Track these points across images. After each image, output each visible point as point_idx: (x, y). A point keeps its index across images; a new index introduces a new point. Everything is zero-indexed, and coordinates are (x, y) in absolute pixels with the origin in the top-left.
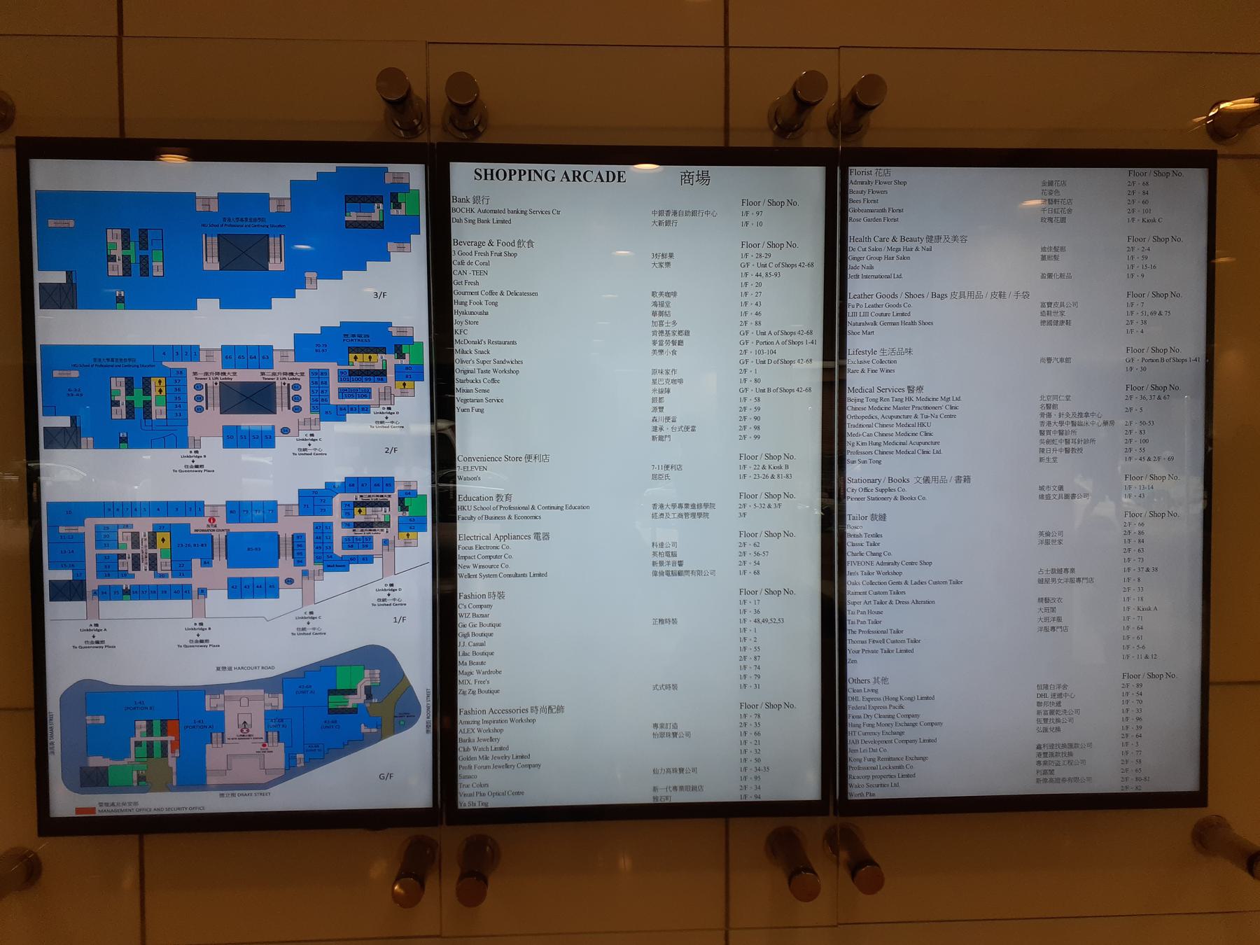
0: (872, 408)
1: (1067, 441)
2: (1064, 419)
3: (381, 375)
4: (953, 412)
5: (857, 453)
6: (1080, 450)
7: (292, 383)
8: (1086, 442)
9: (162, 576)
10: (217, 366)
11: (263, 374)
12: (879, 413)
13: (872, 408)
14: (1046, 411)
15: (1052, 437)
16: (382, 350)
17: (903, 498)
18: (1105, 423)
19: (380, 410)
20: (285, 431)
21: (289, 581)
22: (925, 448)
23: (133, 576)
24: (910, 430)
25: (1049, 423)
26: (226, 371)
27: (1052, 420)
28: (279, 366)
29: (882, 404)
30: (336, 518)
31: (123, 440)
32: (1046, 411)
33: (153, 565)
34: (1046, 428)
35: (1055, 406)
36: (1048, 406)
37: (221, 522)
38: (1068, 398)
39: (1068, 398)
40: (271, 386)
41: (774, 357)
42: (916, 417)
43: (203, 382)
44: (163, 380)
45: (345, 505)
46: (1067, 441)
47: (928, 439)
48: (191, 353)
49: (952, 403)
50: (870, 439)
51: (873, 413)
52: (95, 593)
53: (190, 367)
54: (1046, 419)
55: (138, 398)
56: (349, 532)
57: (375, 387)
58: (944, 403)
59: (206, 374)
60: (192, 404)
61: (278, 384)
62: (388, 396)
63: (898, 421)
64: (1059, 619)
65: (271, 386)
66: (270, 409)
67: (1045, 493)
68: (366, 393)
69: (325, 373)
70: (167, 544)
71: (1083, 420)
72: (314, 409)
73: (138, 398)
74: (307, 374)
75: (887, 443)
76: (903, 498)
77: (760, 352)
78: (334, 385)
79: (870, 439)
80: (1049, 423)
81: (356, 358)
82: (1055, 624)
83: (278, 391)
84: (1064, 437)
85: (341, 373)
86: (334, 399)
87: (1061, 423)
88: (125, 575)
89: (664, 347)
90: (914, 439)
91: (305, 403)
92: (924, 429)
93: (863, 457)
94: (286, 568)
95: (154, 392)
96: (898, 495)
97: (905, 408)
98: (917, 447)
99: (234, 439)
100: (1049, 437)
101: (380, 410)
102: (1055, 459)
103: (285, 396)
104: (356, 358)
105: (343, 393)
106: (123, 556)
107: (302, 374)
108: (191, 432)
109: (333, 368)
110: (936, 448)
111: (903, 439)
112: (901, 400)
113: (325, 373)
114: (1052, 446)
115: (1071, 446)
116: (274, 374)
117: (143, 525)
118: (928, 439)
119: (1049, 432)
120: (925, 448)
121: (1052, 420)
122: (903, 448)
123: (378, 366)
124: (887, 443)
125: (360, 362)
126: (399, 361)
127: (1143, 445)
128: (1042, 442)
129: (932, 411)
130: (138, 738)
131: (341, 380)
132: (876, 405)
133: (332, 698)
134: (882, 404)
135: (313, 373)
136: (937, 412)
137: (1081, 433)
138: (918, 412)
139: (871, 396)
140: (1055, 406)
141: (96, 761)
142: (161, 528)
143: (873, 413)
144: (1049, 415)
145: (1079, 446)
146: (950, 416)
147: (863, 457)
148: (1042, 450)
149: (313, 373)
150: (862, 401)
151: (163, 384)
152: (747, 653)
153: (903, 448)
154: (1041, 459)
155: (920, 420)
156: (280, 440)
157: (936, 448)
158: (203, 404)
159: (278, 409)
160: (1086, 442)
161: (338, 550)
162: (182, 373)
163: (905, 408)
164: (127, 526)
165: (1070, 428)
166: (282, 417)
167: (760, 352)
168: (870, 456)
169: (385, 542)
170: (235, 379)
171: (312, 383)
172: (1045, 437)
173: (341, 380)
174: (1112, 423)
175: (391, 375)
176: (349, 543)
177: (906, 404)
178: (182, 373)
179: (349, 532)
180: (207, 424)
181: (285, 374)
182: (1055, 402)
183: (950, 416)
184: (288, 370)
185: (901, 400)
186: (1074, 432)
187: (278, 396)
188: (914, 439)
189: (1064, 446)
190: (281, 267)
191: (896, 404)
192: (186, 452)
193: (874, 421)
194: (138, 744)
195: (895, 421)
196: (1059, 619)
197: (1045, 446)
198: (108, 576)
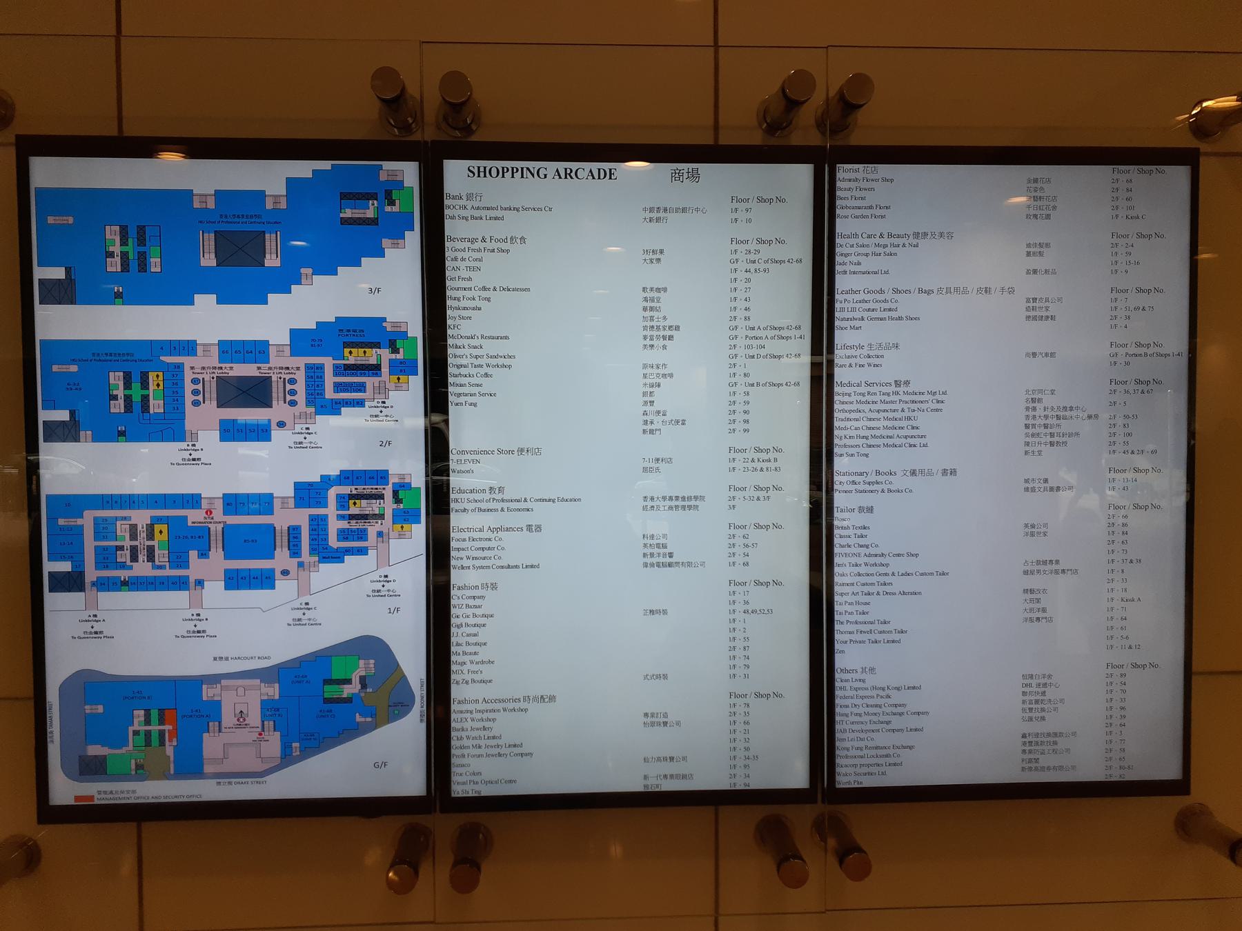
1: (1052, 435)
2: (1049, 413)
3: (375, 369)
4: (939, 406)
5: (845, 446)
6: (1065, 443)
7: (288, 377)
8: (1070, 435)
9: (160, 567)
10: (214, 360)
11: (259, 368)
12: (866, 407)
14: (1031, 405)
15: (1037, 430)
16: (377, 345)
17: (890, 491)
18: (1090, 417)
19: (375, 403)
20: (281, 425)
21: (285, 573)
22: (912, 441)
23: (131, 568)
24: (897, 424)
25: (1034, 417)
26: (223, 365)
27: (1037, 414)
28: (275, 361)
29: (869, 398)
30: (331, 510)
32: (1031, 405)
33: (151, 557)
34: (1031, 422)
35: (1040, 400)
36: (1033, 400)
37: (218, 514)
38: (1053, 392)
39: (1053, 392)
40: (267, 380)
41: (763, 352)
42: (903, 410)
43: (200, 377)
44: (161, 374)
45: (340, 497)
46: (1052, 435)
47: (915, 432)
48: (188, 347)
49: (938, 397)
50: (858, 432)
51: (861, 407)
52: (93, 584)
53: (187, 361)
54: (1031, 413)
55: (136, 392)
56: (344, 524)
57: (370, 381)
58: (931, 397)
59: (203, 368)
60: (189, 398)
61: (274, 378)
62: (382, 390)
63: (885, 414)
64: (1044, 610)
65: (267, 380)
66: (266, 403)
67: (1030, 486)
68: (361, 388)
69: (321, 367)
70: (165, 536)
71: (1068, 413)
72: (309, 403)
73: (136, 392)
74: (303, 369)
75: (875, 437)
76: (890, 491)
77: (749, 347)
78: (330, 379)
79: (858, 432)
80: (1034, 417)
81: (351, 353)
82: (1040, 615)
83: (274, 385)
84: (1049, 431)
85: (336, 367)
86: (329, 393)
87: (1046, 417)
88: (123, 566)
89: (655, 342)
90: (901, 433)
91: (301, 397)
92: (910, 423)
93: (851, 451)
94: (282, 559)
95: (152, 386)
96: (886, 487)
97: (892, 402)
98: (904, 441)
100: (1034, 431)
101: (375, 403)
102: (1040, 453)
103: (281, 390)
104: (351, 353)
105: (339, 387)
106: (121, 548)
107: (298, 368)
109: (328, 363)
110: (923, 441)
111: (890, 433)
112: (888, 394)
113: (321, 367)
114: (1037, 440)
115: (1056, 439)
116: (270, 368)
117: (141, 518)
118: (915, 432)
119: (1034, 426)
120: (912, 441)
121: (1037, 414)
122: (890, 441)
123: (373, 361)
124: (875, 437)
125: (354, 356)
126: (393, 356)
127: (1127, 439)
128: (1027, 435)
129: (919, 405)
130: (136, 727)
131: (336, 375)
132: (864, 399)
134: (869, 398)
135: (309, 367)
136: (924, 406)
137: (1066, 426)
138: (905, 406)
139: (859, 390)
140: (1040, 400)
141: (94, 750)
142: (159, 520)
143: (861, 407)
144: (1034, 409)
145: (1064, 439)
146: (937, 410)
147: (851, 451)
148: (1027, 444)
149: (309, 367)
150: (849, 395)
151: (161, 378)
153: (890, 441)
154: (1026, 453)
155: (907, 414)
157: (923, 441)
158: (200, 398)
159: (274, 403)
160: (1070, 435)
161: (333, 542)
162: (179, 367)
163: (892, 402)
164: (125, 518)
165: (1055, 421)
166: (278, 411)
167: (749, 347)
168: (857, 450)
169: (380, 534)
170: (231, 374)
171: (307, 377)
172: (1031, 431)
173: (336, 375)
174: (1096, 416)
175: (385, 369)
176: (344, 535)
177: (893, 398)
178: (179, 367)
179: (344, 524)
180: (204, 418)
181: (281, 368)
182: (1040, 396)
183: (937, 410)
184: (284, 364)
185: (888, 394)
186: (1058, 425)
187: (274, 390)
188: (901, 433)
189: (1049, 439)
190: (277, 263)
191: (883, 398)
193: (861, 415)
194: (136, 733)
195: (882, 415)
196: (1044, 610)
197: (1030, 440)
198: (106, 567)
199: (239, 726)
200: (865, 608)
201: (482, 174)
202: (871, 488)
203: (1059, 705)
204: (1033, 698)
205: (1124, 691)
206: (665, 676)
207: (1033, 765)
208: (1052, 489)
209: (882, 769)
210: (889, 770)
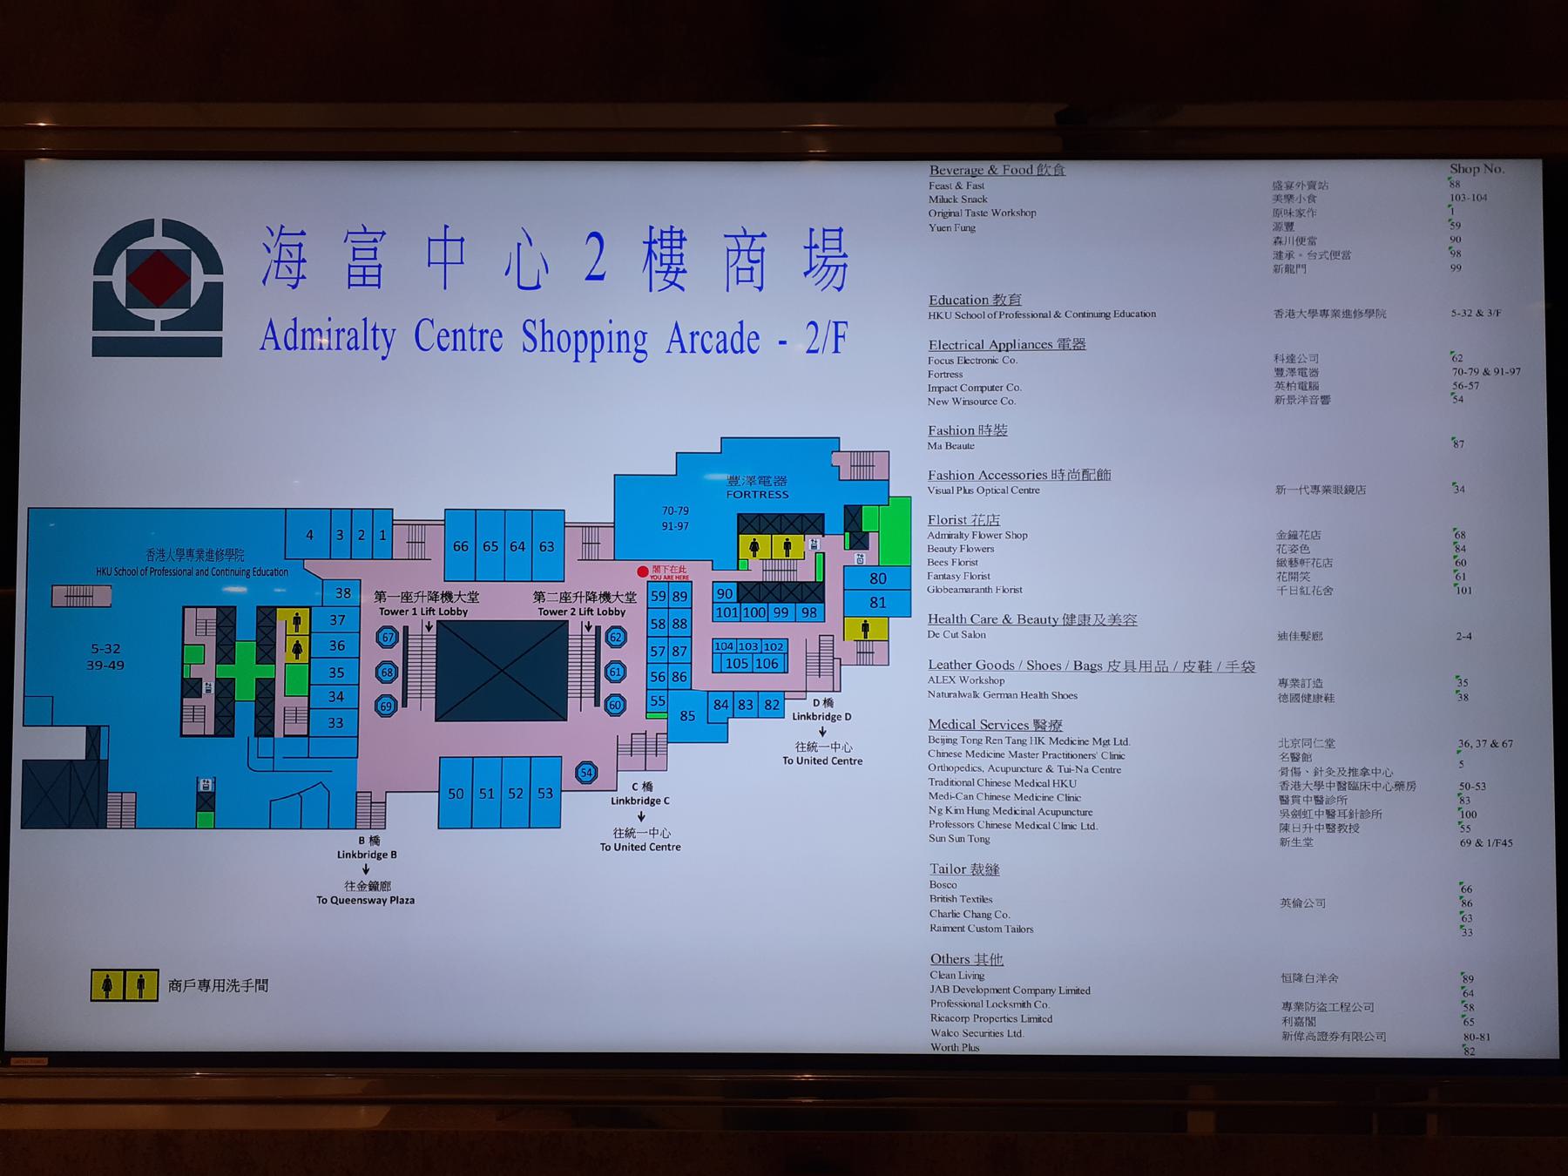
1: (1330, 814)
2: (1325, 779)
3: (812, 593)
4: (1115, 764)
5: (947, 825)
6: (1356, 828)
7: (606, 623)
8: (1363, 814)
10: (429, 576)
11: (539, 596)
12: (984, 763)
15: (1303, 806)
16: (811, 524)
18: (1399, 785)
19: (805, 707)
20: (587, 774)
22: (1068, 820)
24: (1039, 791)
25: (1297, 785)
26: (454, 588)
27: (1302, 779)
28: (581, 576)
29: (990, 748)
31: (206, 802)
34: (1290, 793)
35: (1306, 757)
36: (1294, 757)
38: (1330, 743)
39: (1330, 743)
40: (556, 631)
42: (1049, 770)
43: (398, 623)
44: (304, 614)
46: (1330, 814)
47: (1071, 806)
48: (366, 531)
50: (970, 803)
51: (975, 762)
53: (371, 574)
54: (1290, 779)
55: (246, 672)
58: (1099, 749)
59: (406, 597)
60: (371, 688)
61: (574, 629)
62: (826, 663)
63: (1019, 776)
65: (556, 631)
66: (549, 705)
68: (773, 656)
71: (1359, 779)
72: (655, 703)
73: (246, 672)
74: (641, 598)
75: (1000, 811)
78: (706, 629)
79: (970, 803)
80: (1297, 785)
81: (754, 547)
83: (573, 644)
84: (1323, 808)
85: (719, 591)
86: (704, 677)
87: (1319, 785)
90: (1047, 806)
91: (634, 688)
92: (1064, 790)
95: (283, 654)
97: (1030, 755)
98: (1052, 819)
99: (470, 800)
100: (1296, 807)
101: (805, 707)
102: (1308, 842)
103: (589, 658)
104: (754, 547)
105: (729, 655)
107: (631, 597)
108: (367, 775)
110: (1086, 820)
111: (1027, 805)
112: (1023, 743)
114: (1302, 821)
115: (1337, 821)
116: (565, 597)
118: (1071, 806)
119: (1296, 799)
120: (1068, 820)
121: (1302, 779)
122: (1028, 820)
123: (805, 574)
124: (1000, 811)
125: (766, 558)
126: (855, 556)
128: (1284, 813)
129: (1079, 762)
131: (719, 615)
132: (979, 749)
134: (990, 748)
136: (1087, 763)
137: (1356, 800)
138: (1054, 763)
139: (970, 735)
140: (1306, 757)
143: (975, 762)
145: (1353, 821)
146: (1111, 771)
147: (957, 833)
148: (1286, 828)
150: (954, 742)
151: (304, 627)
153: (1028, 820)
154: (1283, 842)
155: (1057, 775)
156: (573, 803)
158: (395, 689)
159: (572, 703)
160: (1363, 814)
162: (348, 589)
163: (1030, 755)
165: (1335, 792)
166: (582, 730)
168: (969, 831)
170: (476, 613)
171: (654, 624)
172: (1291, 807)
173: (719, 615)
174: (1412, 785)
175: (833, 593)
178: (348, 589)
180: (411, 741)
181: (591, 597)
182: (1306, 750)
183: (1111, 771)
184: (594, 591)
185: (1023, 743)
186: (1342, 799)
187: (573, 658)
188: (1047, 806)
189: (1324, 820)
192: (347, 839)
193: (976, 775)
195: (1011, 777)
197: (1290, 821)
206: (1334, 978)
207: (1306, 1029)
209: (1013, 1027)
210: (1027, 1029)
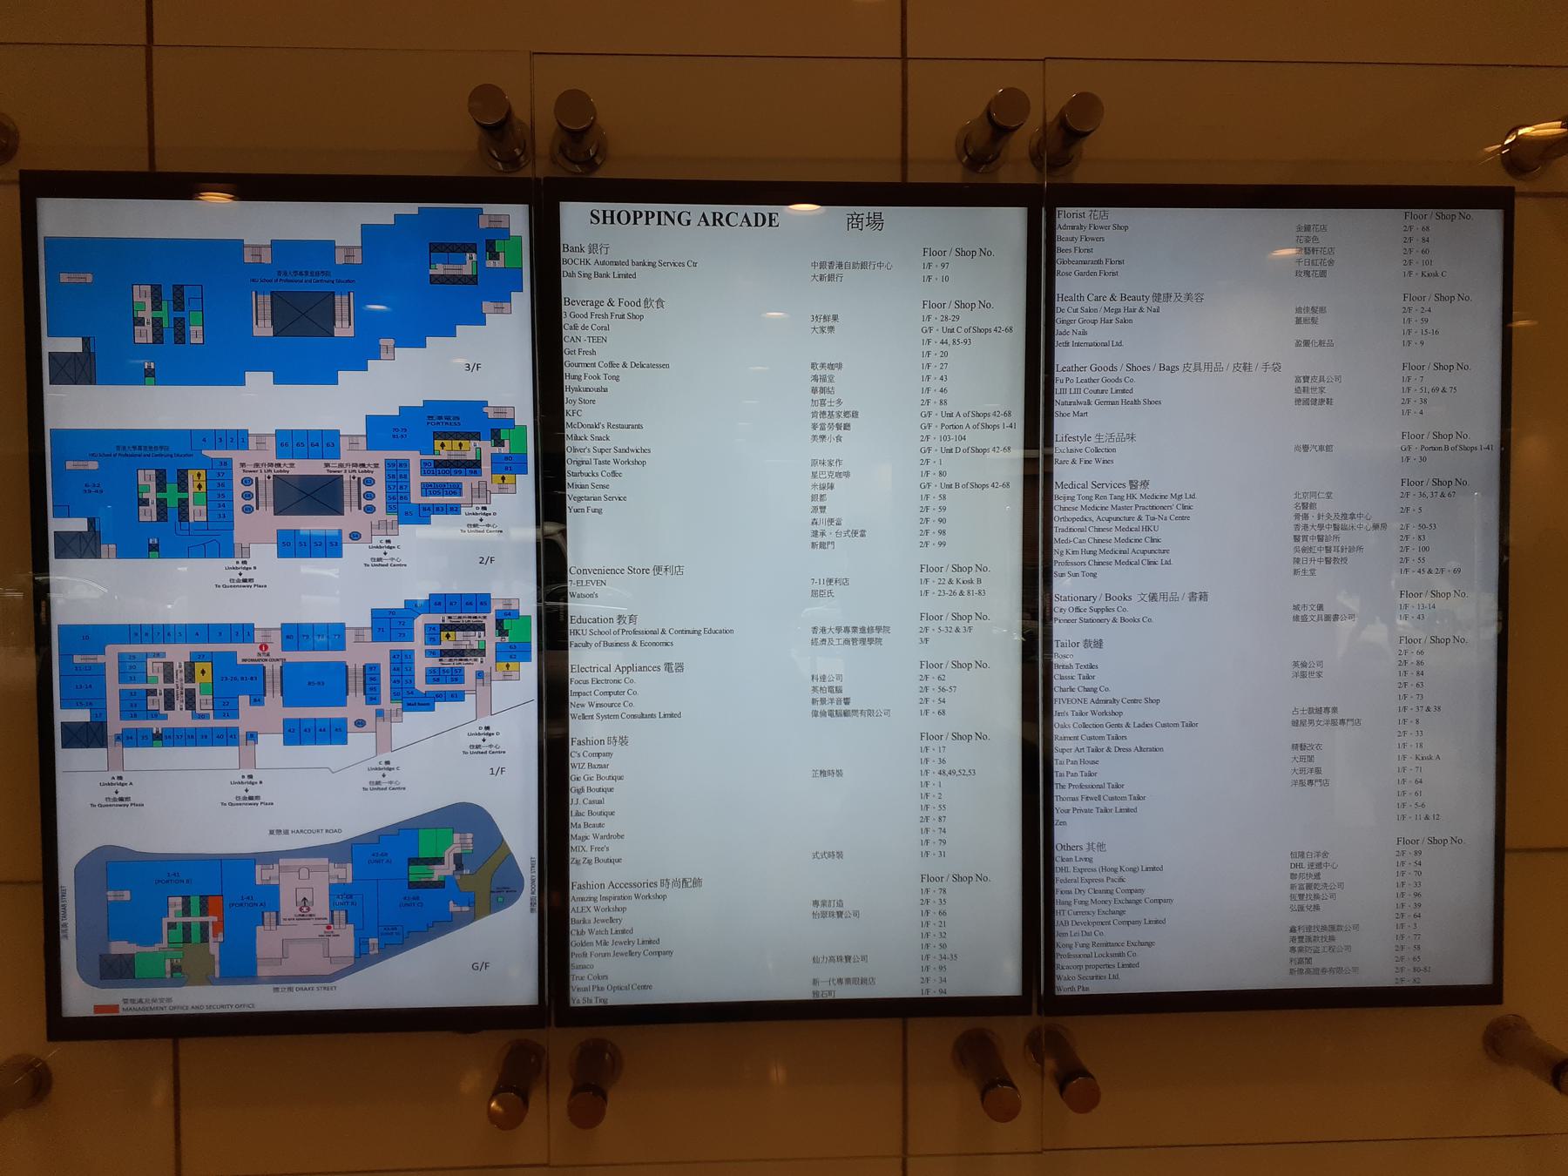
0: (1086, 508)
1: (1328, 549)
2: (1324, 521)
3: (474, 466)
4: (1186, 513)
5: (1067, 563)
6: (1344, 560)
7: (363, 476)
8: (1351, 549)
9: (202, 717)
10: (270, 455)
11: (327, 465)
12: (1093, 514)
13: (1086, 508)
14: (1302, 512)
15: (1309, 543)
16: (476, 436)
17: (1123, 620)
18: (1376, 527)
19: (473, 510)
20: (355, 536)
21: (360, 723)
22: (1151, 557)
23: (165, 717)
24: (1132, 535)
25: (1306, 527)
26: (282, 462)
27: (1309, 522)
28: (347, 455)
29: (1098, 503)
30: (418, 645)
31: (153, 548)
32: (1302, 512)
33: (190, 704)
34: (1301, 533)
35: (1313, 506)
36: (1304, 506)
37: (275, 650)
38: (1329, 495)
39: (1329, 495)
40: (337, 480)
42: (1140, 518)
43: (253, 476)
44: (203, 473)
45: (429, 628)
46: (1328, 549)
47: (1155, 546)
48: (238, 439)
49: (1185, 502)
50: (1083, 546)
51: (1087, 514)
52: (118, 738)
53: (237, 456)
54: (1302, 522)
55: (172, 496)
56: (434, 662)
57: (467, 482)
58: (1175, 501)
59: (257, 465)
60: (238, 502)
61: (346, 478)
62: (483, 493)
63: (1118, 524)
64: (1318, 771)
65: (337, 480)
66: (336, 509)
68: (456, 489)
69: (405, 464)
70: (208, 677)
71: (1348, 522)
72: (390, 509)
73: (172, 496)
74: (382, 466)
75: (1104, 552)
76: (1123, 620)
77: (945, 438)
78: (416, 479)
79: (1083, 546)
80: (1306, 527)
81: (443, 445)
82: (1313, 776)
83: (346, 486)
84: (1324, 544)
85: (424, 464)
86: (416, 497)
87: (1321, 527)
88: (155, 715)
89: (826, 432)
90: (1138, 546)
91: (380, 502)
92: (1149, 534)
93: (1074, 569)
94: (356, 706)
95: (192, 488)
96: (1118, 615)
97: (1126, 508)
98: (1141, 557)
99: (291, 546)
100: (1305, 544)
101: (473, 510)
102: (1313, 572)
103: (355, 492)
104: (443, 445)
105: (427, 489)
106: (153, 692)
107: (376, 465)
108: (238, 537)
109: (414, 458)
110: (1165, 557)
111: (1124, 546)
112: (1121, 498)
113: (405, 464)
114: (1309, 555)
115: (1333, 554)
116: (341, 465)
117: (178, 654)
118: (1155, 546)
119: (1305, 538)
120: (1151, 557)
121: (1309, 522)
122: (1124, 558)
123: (471, 456)
124: (1104, 552)
125: (447, 450)
126: (497, 450)
127: (1422, 554)
128: (1296, 549)
129: (1160, 512)
130: (172, 919)
131: (424, 473)
132: (1090, 504)
133: (413, 869)
134: (1098, 503)
135: (390, 464)
136: (1166, 513)
137: (1345, 538)
138: (1143, 513)
139: (1084, 492)
140: (1313, 506)
141: (119, 948)
142: (201, 657)
143: (1087, 514)
144: (1306, 516)
145: (1343, 555)
146: (1183, 518)
147: (1074, 569)
148: (1297, 561)
149: (390, 464)
150: (1072, 499)
151: (203, 477)
152: (930, 813)
153: (1124, 558)
154: (1296, 572)
155: (1144, 523)
156: (348, 548)
157: (1165, 557)
158: (253, 502)
159: (347, 509)
160: (1351, 549)
161: (421, 685)
162: (226, 464)
163: (1126, 508)
164: (157, 655)
165: (1332, 532)
166: (351, 519)
167: (945, 438)
168: (1082, 568)
169: (480, 675)
170: (292, 472)
171: (388, 476)
172: (1301, 544)
173: (424, 473)
174: (1384, 526)
175: (486, 466)
176: (434, 675)
177: (1127, 503)
178: (226, 464)
179: (434, 662)
180: (258, 528)
181: (355, 465)
182: (1313, 500)
183: (1183, 518)
184: (358, 460)
185: (1121, 498)
186: (1336, 537)
187: (346, 492)
188: (1138, 546)
189: (1324, 554)
191: (1115, 502)
192: (231, 562)
193: (1088, 524)
194: (172, 926)
195: (1114, 524)
196: (1318, 771)
197: (1300, 555)
198: (134, 717)
199: (302, 917)
200: (1093, 768)
201: (608, 220)
202: (1100, 616)
203: (1337, 890)
204: (1304, 882)
205: (1419, 873)
208: (1328, 618)
